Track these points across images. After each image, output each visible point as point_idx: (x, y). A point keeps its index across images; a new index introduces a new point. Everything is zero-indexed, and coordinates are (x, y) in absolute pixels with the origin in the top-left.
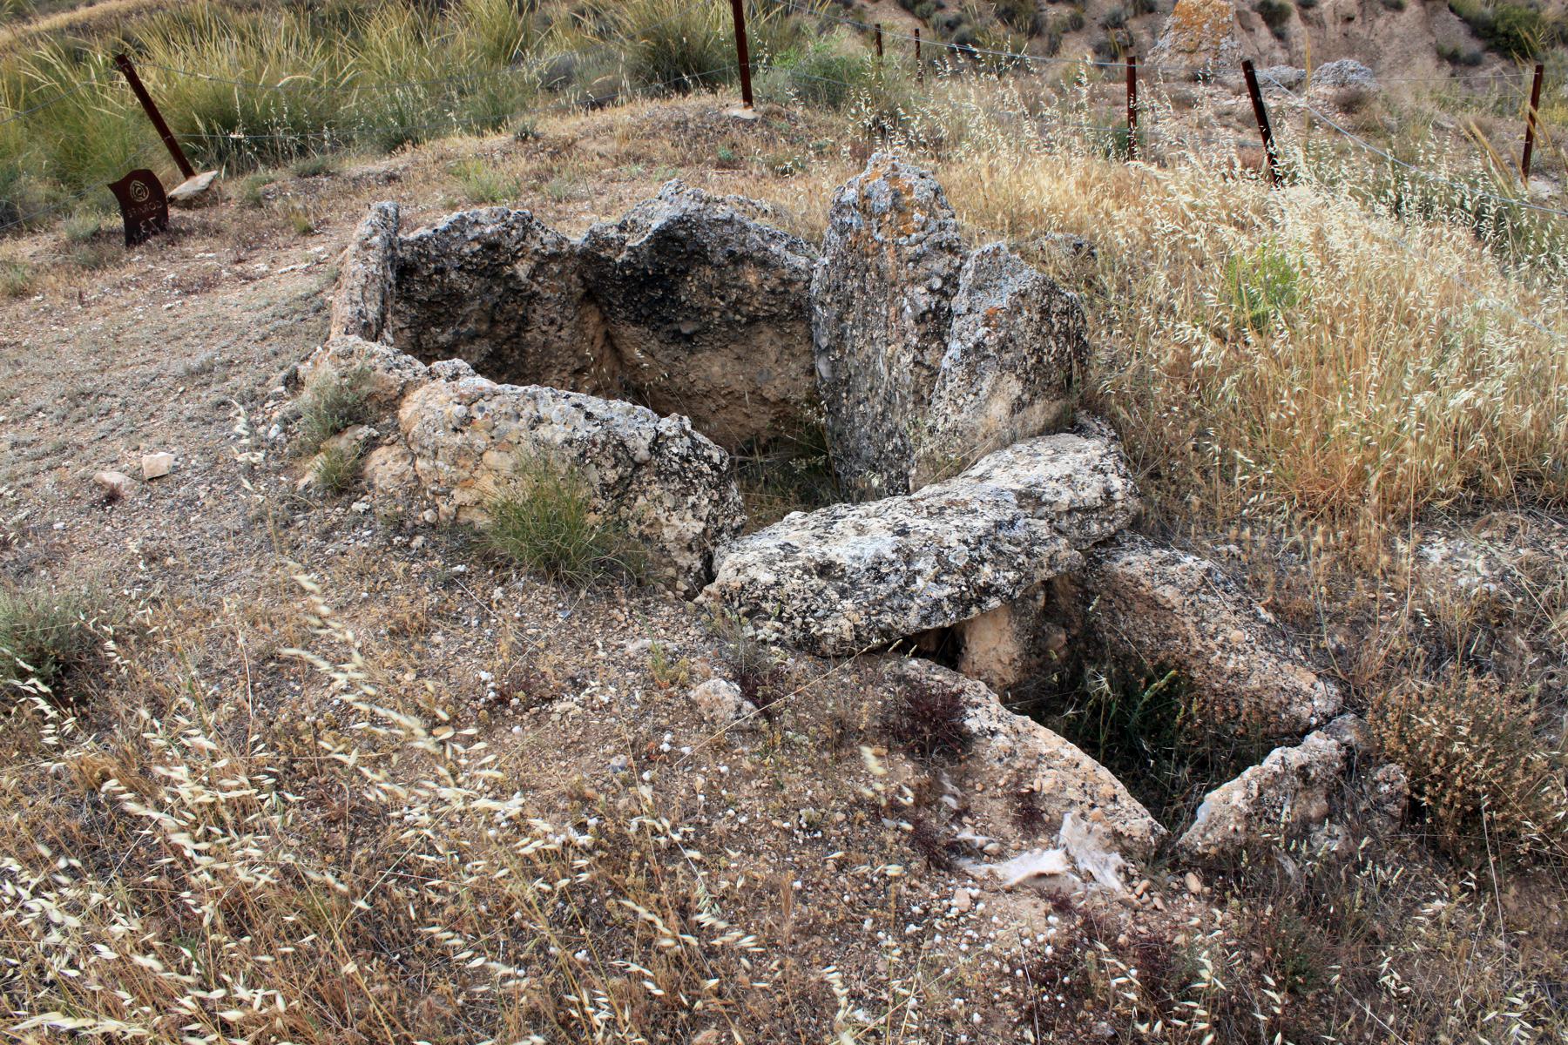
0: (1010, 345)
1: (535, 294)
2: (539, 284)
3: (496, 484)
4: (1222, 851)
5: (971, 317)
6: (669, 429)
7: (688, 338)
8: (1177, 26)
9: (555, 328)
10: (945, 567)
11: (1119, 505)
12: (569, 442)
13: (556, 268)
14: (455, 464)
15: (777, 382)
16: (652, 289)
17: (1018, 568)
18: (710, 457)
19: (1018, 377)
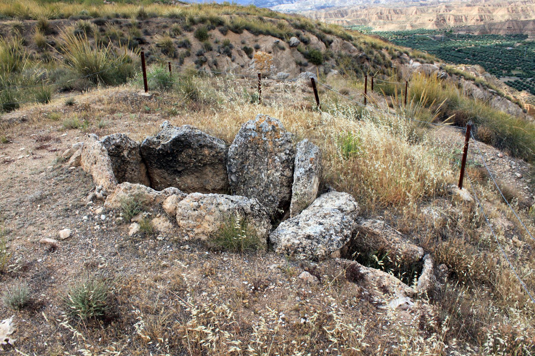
3: (209, 225)
5: (306, 161)
7: (180, 172)
8: (256, 61)
10: (336, 232)
12: (229, 210)
14: (196, 220)
15: (211, 184)
16: (168, 157)
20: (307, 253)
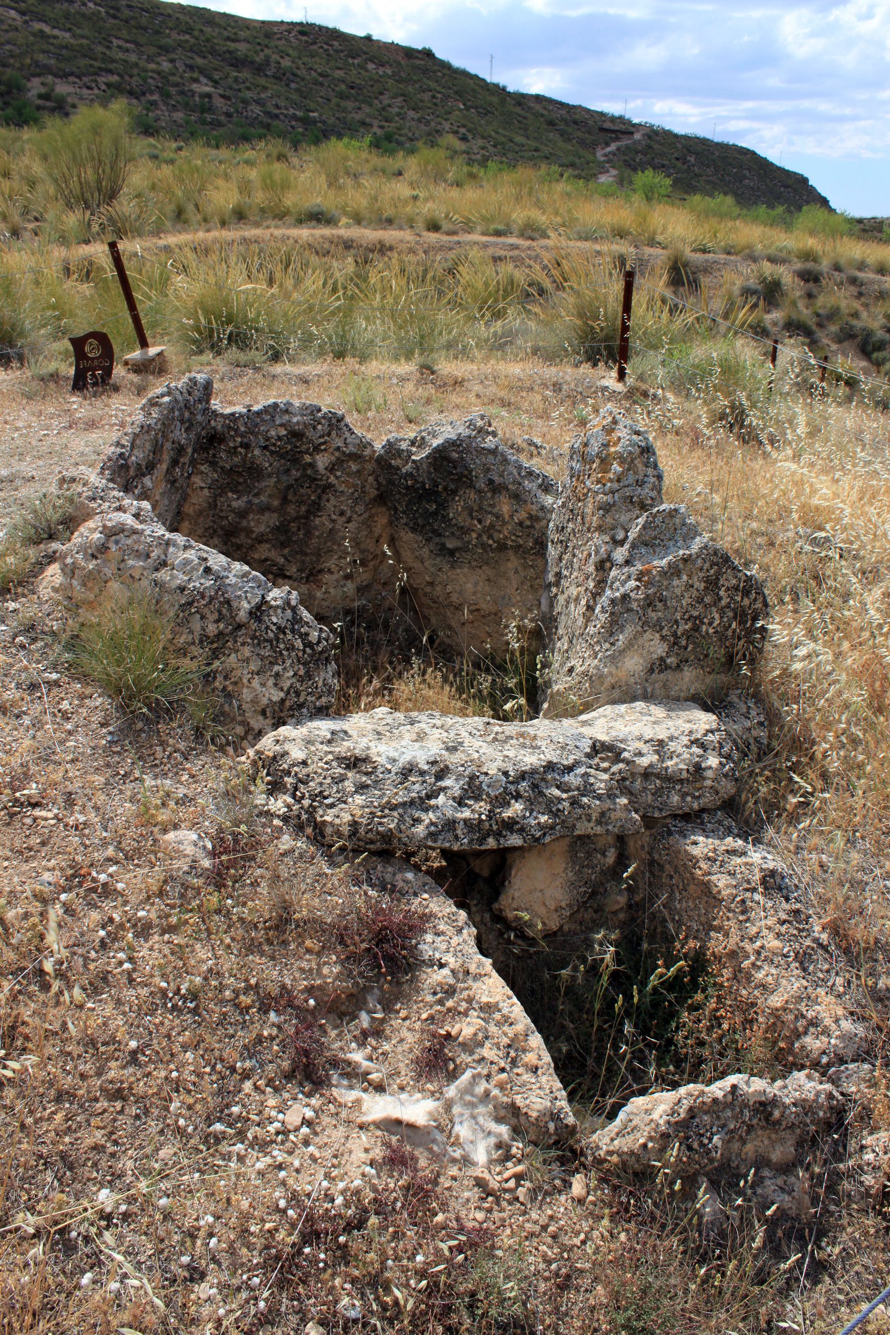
0: (660, 605)
1: (330, 486)
2: (337, 477)
4: (624, 1163)
6: (275, 599)
7: (452, 553)
9: (344, 519)
11: (708, 783)
12: (182, 589)
13: (354, 467)
14: (85, 585)
16: (428, 501)
17: (555, 814)
18: (307, 634)
19: (663, 638)
20: (299, 801)
